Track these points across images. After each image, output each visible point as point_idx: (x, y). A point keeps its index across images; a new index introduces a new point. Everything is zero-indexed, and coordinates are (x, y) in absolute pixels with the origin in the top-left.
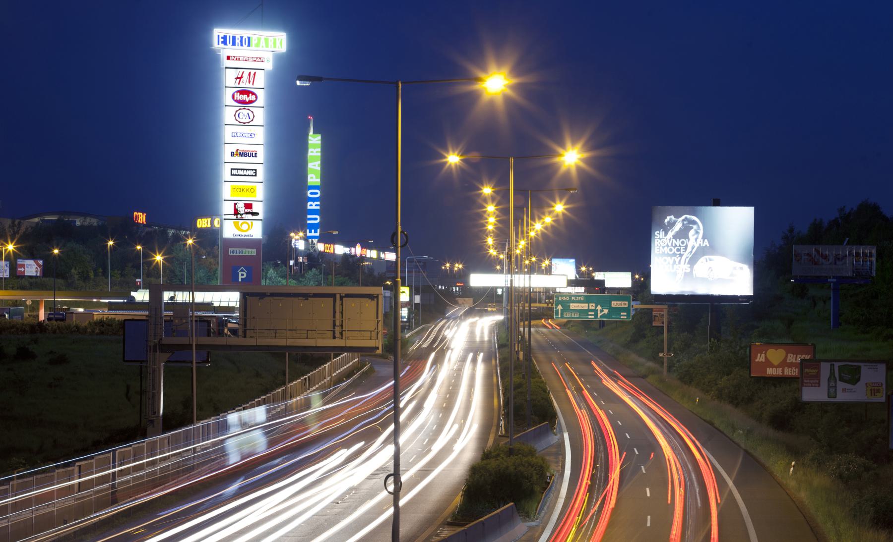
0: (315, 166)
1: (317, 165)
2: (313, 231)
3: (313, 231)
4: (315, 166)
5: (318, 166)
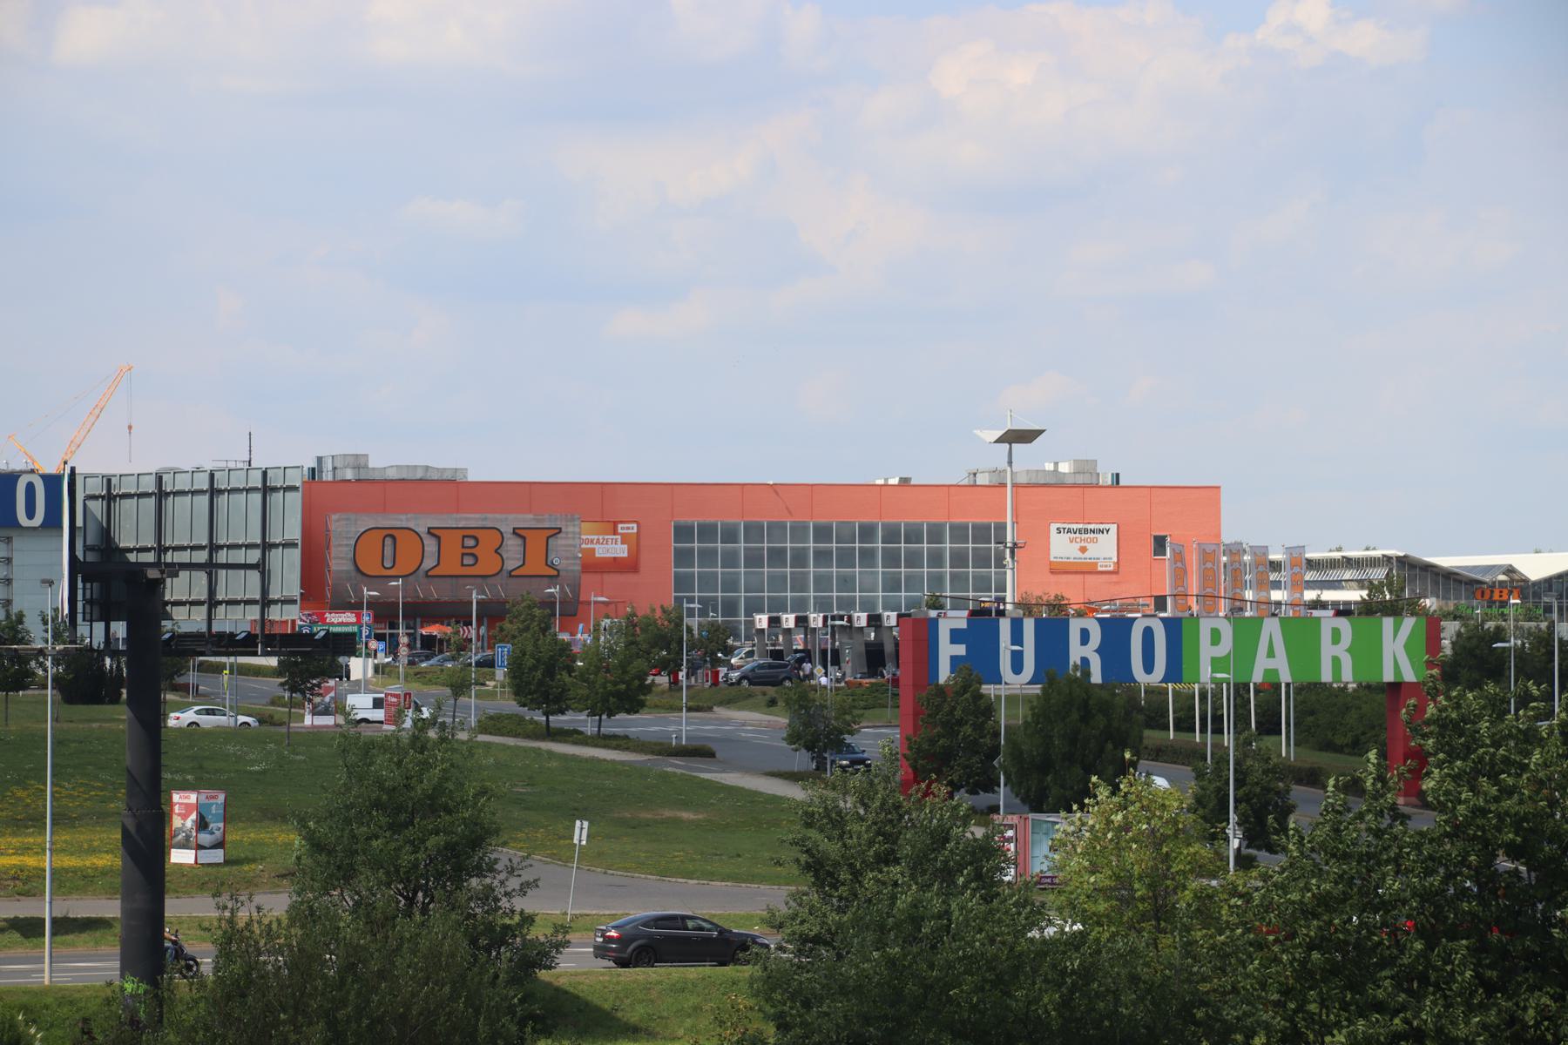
0: (1271, 653)
1: (1271, 664)
2: (961, 650)
3: (961, 650)
4: (1271, 653)
5: (1266, 671)
